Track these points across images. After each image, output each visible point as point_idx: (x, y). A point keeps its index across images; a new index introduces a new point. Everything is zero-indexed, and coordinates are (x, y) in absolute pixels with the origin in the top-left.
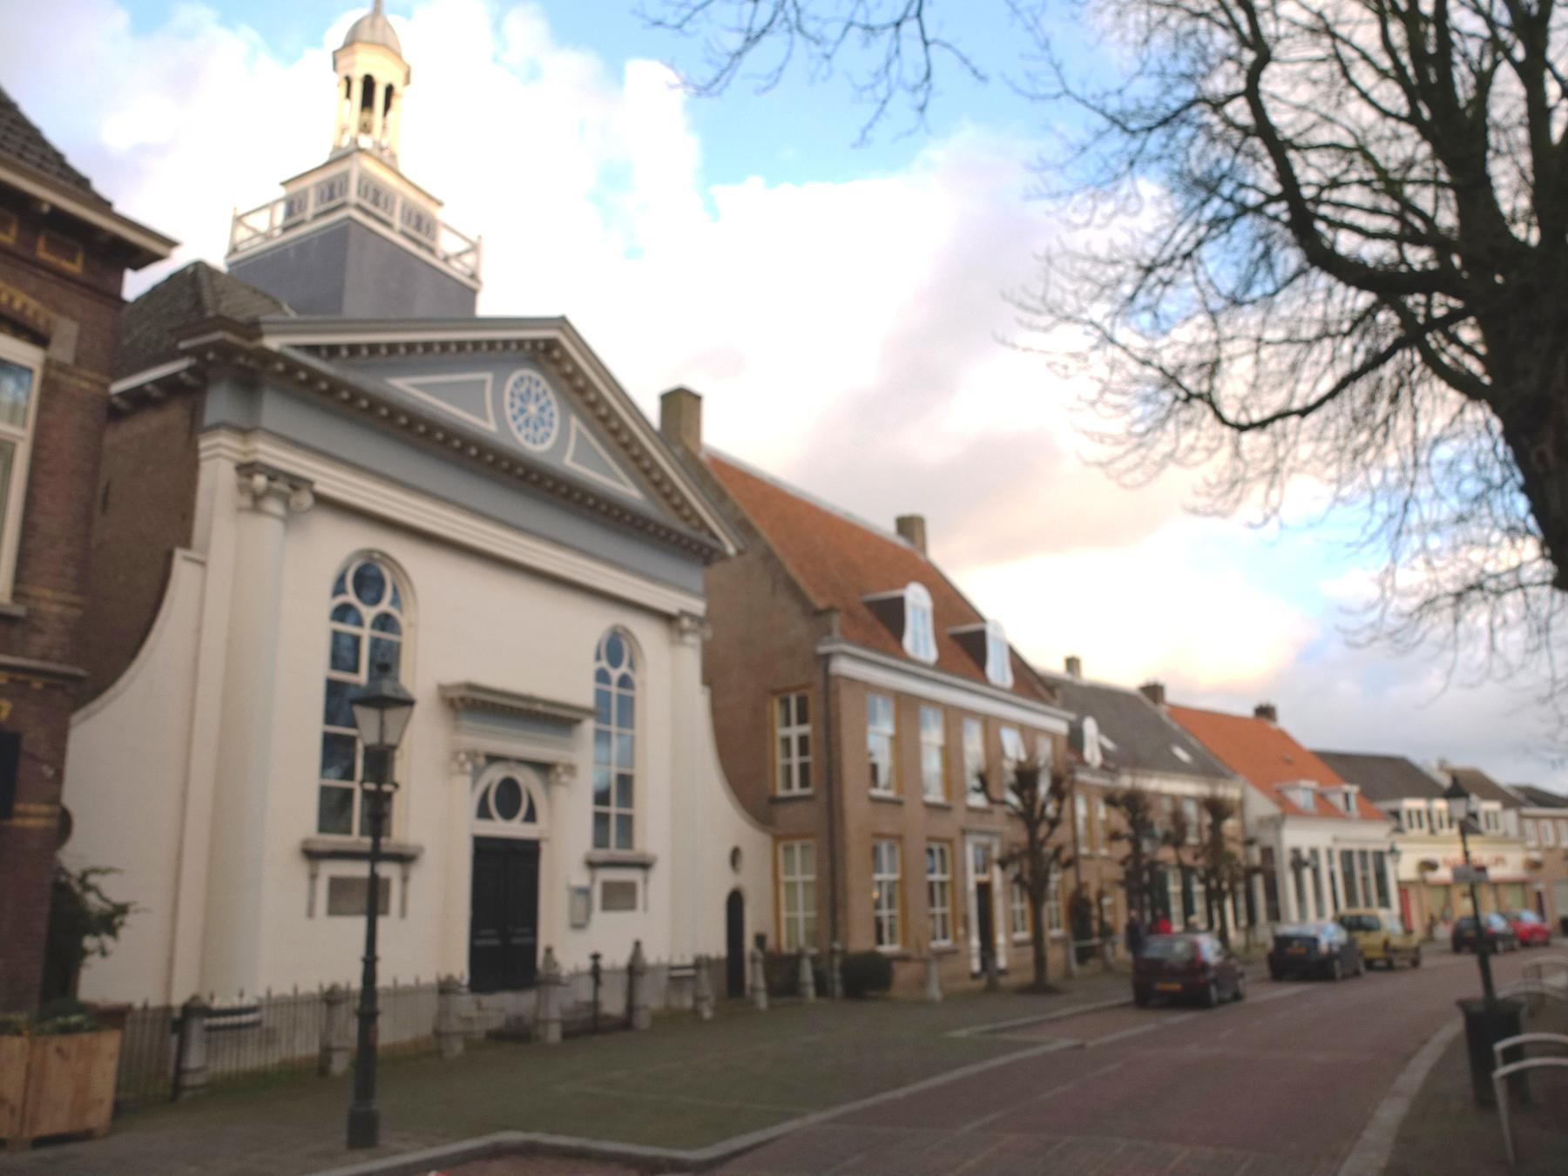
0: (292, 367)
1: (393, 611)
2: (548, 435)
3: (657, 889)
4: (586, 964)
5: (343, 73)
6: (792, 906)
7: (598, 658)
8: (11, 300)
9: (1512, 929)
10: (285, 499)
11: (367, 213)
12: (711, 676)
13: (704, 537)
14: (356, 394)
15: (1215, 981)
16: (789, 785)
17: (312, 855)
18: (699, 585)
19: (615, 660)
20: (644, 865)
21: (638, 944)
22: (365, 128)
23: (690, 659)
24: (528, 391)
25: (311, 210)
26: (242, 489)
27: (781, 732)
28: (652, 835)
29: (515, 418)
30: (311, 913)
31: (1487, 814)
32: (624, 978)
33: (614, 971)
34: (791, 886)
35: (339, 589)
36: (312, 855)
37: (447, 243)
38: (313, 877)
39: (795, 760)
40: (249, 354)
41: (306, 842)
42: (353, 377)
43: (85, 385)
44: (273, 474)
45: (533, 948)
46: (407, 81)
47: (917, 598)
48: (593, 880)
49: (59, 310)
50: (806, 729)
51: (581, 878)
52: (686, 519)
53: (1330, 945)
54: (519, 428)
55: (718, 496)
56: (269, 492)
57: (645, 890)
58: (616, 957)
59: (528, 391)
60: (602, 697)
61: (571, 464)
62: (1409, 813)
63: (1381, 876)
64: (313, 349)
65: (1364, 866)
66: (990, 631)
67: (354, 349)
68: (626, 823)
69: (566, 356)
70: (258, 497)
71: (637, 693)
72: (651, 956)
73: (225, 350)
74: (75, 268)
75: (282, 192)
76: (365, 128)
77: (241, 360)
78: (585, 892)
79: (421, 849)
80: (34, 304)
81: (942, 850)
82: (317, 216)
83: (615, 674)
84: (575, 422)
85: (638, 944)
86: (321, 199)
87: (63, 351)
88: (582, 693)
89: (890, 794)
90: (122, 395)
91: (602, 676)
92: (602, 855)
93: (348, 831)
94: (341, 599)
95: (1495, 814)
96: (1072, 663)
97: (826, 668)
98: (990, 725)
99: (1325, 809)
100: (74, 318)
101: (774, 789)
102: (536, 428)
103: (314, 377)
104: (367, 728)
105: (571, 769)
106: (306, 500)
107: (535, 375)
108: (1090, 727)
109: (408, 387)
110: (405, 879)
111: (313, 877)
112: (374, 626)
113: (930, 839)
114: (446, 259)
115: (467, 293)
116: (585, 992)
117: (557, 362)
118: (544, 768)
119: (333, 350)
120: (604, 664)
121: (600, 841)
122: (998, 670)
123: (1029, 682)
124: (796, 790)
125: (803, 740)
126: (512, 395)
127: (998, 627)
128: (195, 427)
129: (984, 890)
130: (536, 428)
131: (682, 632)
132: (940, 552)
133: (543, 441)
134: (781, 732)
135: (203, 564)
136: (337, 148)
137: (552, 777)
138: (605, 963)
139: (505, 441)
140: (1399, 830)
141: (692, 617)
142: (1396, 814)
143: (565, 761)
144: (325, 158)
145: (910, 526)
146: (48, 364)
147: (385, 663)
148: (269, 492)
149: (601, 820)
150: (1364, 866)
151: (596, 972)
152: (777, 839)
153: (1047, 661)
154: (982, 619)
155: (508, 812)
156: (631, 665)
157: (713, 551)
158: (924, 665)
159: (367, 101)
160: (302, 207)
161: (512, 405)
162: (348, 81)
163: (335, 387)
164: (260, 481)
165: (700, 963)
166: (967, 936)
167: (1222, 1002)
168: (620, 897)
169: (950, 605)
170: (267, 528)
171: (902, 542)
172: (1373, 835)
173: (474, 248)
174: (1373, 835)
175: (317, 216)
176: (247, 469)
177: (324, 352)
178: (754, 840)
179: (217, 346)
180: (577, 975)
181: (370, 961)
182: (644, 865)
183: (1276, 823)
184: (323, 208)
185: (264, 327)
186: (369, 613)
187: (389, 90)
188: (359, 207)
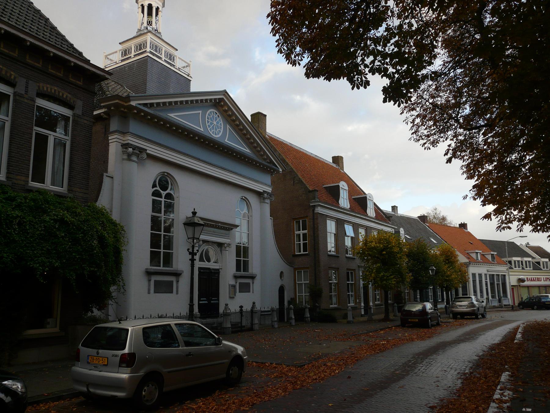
0: (140, 111)
1: (172, 192)
2: (220, 131)
3: (256, 286)
4: (238, 309)
5: (140, 4)
6: (301, 291)
8: (63, 95)
10: (138, 156)
11: (153, 54)
12: (273, 214)
13: (277, 169)
14: (160, 119)
15: (430, 318)
16: (300, 252)
17: (149, 273)
18: (269, 181)
19: (164, 188)
20: (253, 277)
21: (254, 303)
22: (149, 23)
23: (267, 208)
24: (213, 117)
25: (133, 53)
26: (124, 152)
27: (297, 232)
28: (255, 267)
29: (209, 126)
30: (149, 293)
31: (543, 262)
33: (247, 312)
34: (300, 285)
35: (154, 186)
36: (149, 273)
37: (179, 64)
38: (150, 280)
39: (302, 242)
40: (125, 107)
41: (147, 269)
42: (162, 114)
43: (85, 122)
44: (135, 148)
45: (217, 305)
46: (164, 6)
47: (343, 185)
50: (306, 231)
51: (232, 282)
52: (265, 159)
54: (210, 130)
55: (273, 151)
56: (133, 153)
57: (253, 285)
58: (247, 307)
59: (213, 117)
61: (228, 141)
62: (515, 262)
63: (504, 284)
64: (145, 105)
65: (498, 280)
66: (368, 197)
67: (158, 104)
68: (246, 263)
69: (226, 104)
70: (129, 156)
71: (175, 202)
72: (258, 307)
73: (117, 106)
74: (80, 83)
75: (120, 47)
76: (149, 23)
77: (122, 109)
78: (234, 286)
79: (183, 271)
81: (350, 273)
82: (135, 55)
84: (228, 126)
85: (254, 303)
86: (136, 50)
87: (79, 111)
89: (351, 256)
90: (39, 108)
93: (160, 266)
95: (547, 262)
96: (394, 208)
97: (314, 210)
98: (367, 229)
99: (485, 261)
100: (81, 100)
101: (295, 252)
102: (216, 130)
103: (147, 114)
106: (145, 156)
107: (215, 111)
108: (402, 231)
109: (174, 116)
110: (178, 282)
111: (150, 280)
113: (347, 269)
114: (179, 69)
115: (187, 82)
116: (236, 319)
117: (222, 106)
118: (220, 245)
119: (152, 105)
121: (238, 269)
122: (371, 212)
123: (381, 216)
124: (302, 253)
125: (304, 235)
126: (208, 118)
127: (371, 196)
128: (107, 132)
129: (366, 288)
131: (264, 199)
132: (348, 169)
133: (218, 134)
134: (297, 232)
136: (140, 30)
137: (223, 248)
138: (244, 309)
139: (206, 134)
140: (511, 268)
141: (268, 193)
142: (510, 262)
144: (135, 34)
145: (337, 160)
146: (74, 115)
148: (133, 153)
149: (238, 262)
150: (498, 280)
152: (295, 269)
153: (386, 208)
154: (365, 194)
157: (274, 170)
159: (150, 14)
160: (130, 52)
161: (208, 122)
162: (143, 6)
163: (153, 117)
164: (130, 150)
165: (272, 310)
166: (360, 303)
167: (433, 326)
168: (245, 288)
169: (354, 188)
170: (133, 166)
171: (334, 165)
172: (501, 269)
173: (188, 66)
174: (501, 269)
176: (125, 146)
177: (149, 106)
178: (286, 268)
179: (114, 105)
182: (253, 277)
183: (467, 265)
185: (131, 98)
186: (164, 193)
187: (157, 9)
188: (151, 53)
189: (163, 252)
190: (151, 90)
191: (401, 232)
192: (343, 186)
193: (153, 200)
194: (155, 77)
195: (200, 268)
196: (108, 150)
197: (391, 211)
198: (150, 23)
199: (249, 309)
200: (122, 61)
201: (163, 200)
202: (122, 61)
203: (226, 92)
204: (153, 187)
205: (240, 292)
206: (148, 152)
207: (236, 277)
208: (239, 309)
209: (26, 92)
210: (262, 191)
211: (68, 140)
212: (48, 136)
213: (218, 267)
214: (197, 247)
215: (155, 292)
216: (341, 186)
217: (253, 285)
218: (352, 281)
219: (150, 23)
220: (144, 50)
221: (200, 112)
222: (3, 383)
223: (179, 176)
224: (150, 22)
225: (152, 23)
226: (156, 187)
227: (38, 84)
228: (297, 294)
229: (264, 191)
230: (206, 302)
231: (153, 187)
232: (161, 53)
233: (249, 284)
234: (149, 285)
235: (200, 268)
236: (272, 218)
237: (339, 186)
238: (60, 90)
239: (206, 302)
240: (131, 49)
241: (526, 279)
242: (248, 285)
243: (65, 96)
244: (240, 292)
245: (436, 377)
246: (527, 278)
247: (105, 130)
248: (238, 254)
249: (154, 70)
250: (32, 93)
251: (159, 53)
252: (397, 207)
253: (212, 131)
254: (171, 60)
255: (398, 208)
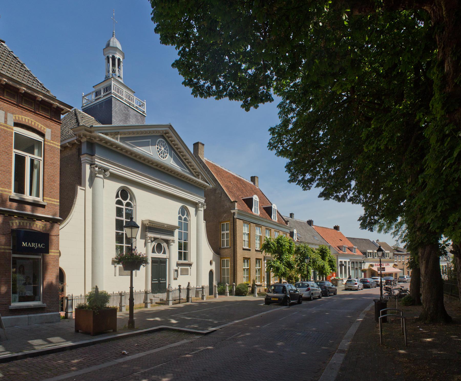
2: (167, 156)
5: (106, 56)
7: (179, 214)
9: (100, 294)
21: (189, 283)
31: (387, 253)
32: (186, 291)
35: (117, 196)
39: (225, 239)
48: (178, 268)
49: (47, 127)
53: (169, 45)
57: (190, 270)
60: (180, 223)
78: (177, 271)
80: (40, 125)
82: (104, 96)
83: (183, 217)
85: (189, 283)
88: (175, 223)
91: (180, 218)
92: (181, 262)
94: (118, 199)
95: (389, 253)
102: (164, 154)
104: (126, 231)
105: (173, 241)
112: (126, 206)
120: (180, 215)
121: (180, 258)
124: (225, 246)
130: (164, 154)
132: (261, 185)
133: (165, 158)
135: (85, 190)
143: (172, 239)
144: (104, 79)
147: (129, 216)
149: (180, 253)
151: (180, 289)
152: (221, 258)
155: (159, 251)
156: (187, 215)
158: (275, 222)
162: (108, 58)
168: (185, 272)
175: (104, 96)
180: (175, 290)
181: (131, 288)
182: (190, 265)
184: (105, 94)
186: (125, 202)
189: (182, 250)
190: (116, 123)
191: (294, 232)
192: (256, 199)
193: (117, 208)
194: (118, 113)
195: (152, 258)
196: (81, 169)
197: (289, 217)
198: (114, 71)
199: (186, 287)
200: (96, 100)
201: (124, 207)
202: (96, 100)
203: (171, 125)
204: (116, 198)
205: (181, 275)
206: (110, 170)
207: (178, 265)
208: (178, 287)
209: (6, 122)
210: (198, 202)
211: (41, 160)
212: (25, 157)
213: (166, 257)
214: (149, 242)
215: (120, 275)
216: (254, 199)
217: (190, 270)
218: (259, 267)
219: (114, 71)
220: (109, 92)
221: (150, 140)
222: (30, 342)
223: (135, 190)
224: (114, 70)
225: (115, 71)
226: (118, 197)
227: (15, 115)
228: (222, 276)
229: (199, 202)
230: (157, 282)
231: (116, 198)
232: (123, 94)
233: (188, 269)
234: (115, 270)
235: (152, 258)
236: (205, 222)
237: (252, 199)
238: (32, 120)
239: (157, 282)
240: (101, 91)
241: (374, 265)
242: (187, 270)
243: (39, 127)
244: (181, 275)
245: (220, 329)
246: (375, 264)
247: (79, 153)
248: (180, 248)
249: (117, 107)
250: (11, 123)
251: (121, 94)
252: (294, 214)
253: (161, 155)
254: (130, 100)
255: (294, 215)
